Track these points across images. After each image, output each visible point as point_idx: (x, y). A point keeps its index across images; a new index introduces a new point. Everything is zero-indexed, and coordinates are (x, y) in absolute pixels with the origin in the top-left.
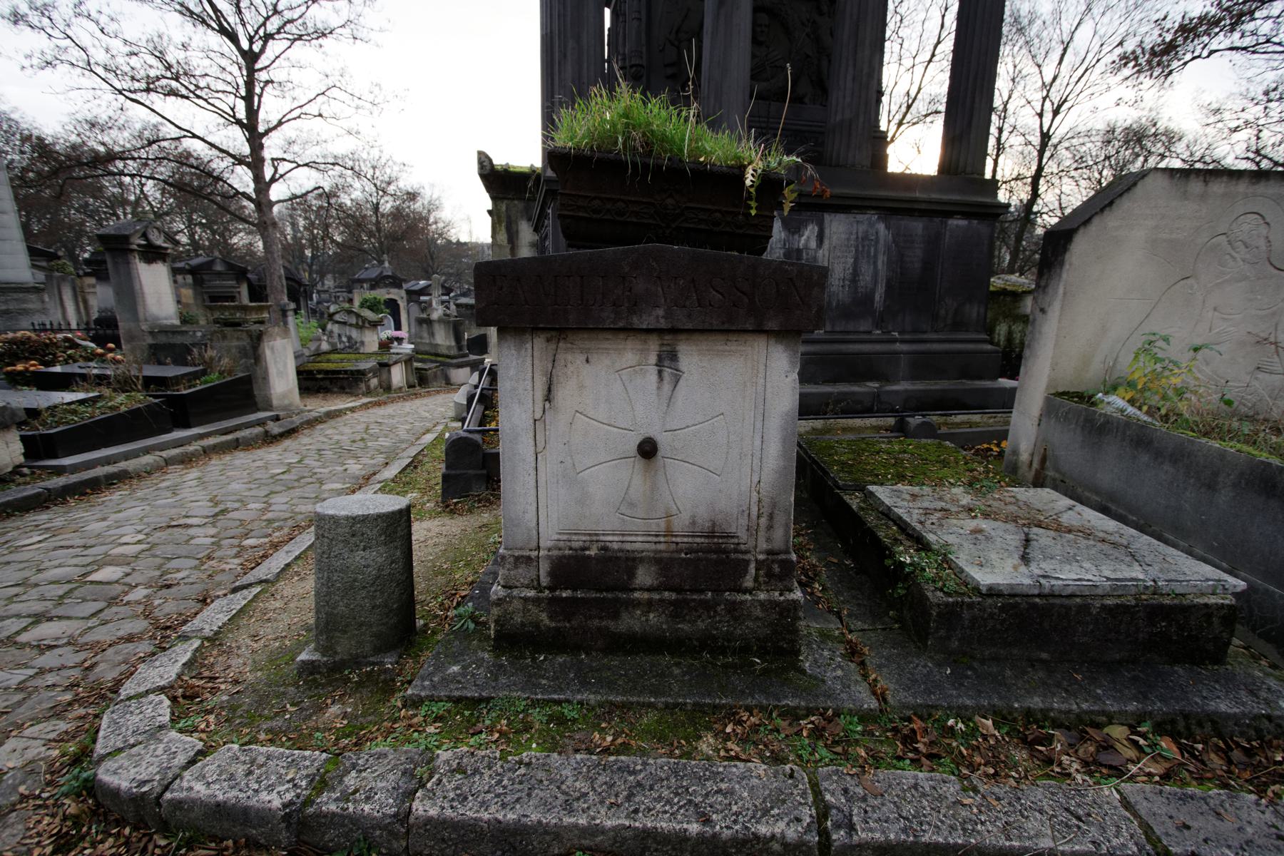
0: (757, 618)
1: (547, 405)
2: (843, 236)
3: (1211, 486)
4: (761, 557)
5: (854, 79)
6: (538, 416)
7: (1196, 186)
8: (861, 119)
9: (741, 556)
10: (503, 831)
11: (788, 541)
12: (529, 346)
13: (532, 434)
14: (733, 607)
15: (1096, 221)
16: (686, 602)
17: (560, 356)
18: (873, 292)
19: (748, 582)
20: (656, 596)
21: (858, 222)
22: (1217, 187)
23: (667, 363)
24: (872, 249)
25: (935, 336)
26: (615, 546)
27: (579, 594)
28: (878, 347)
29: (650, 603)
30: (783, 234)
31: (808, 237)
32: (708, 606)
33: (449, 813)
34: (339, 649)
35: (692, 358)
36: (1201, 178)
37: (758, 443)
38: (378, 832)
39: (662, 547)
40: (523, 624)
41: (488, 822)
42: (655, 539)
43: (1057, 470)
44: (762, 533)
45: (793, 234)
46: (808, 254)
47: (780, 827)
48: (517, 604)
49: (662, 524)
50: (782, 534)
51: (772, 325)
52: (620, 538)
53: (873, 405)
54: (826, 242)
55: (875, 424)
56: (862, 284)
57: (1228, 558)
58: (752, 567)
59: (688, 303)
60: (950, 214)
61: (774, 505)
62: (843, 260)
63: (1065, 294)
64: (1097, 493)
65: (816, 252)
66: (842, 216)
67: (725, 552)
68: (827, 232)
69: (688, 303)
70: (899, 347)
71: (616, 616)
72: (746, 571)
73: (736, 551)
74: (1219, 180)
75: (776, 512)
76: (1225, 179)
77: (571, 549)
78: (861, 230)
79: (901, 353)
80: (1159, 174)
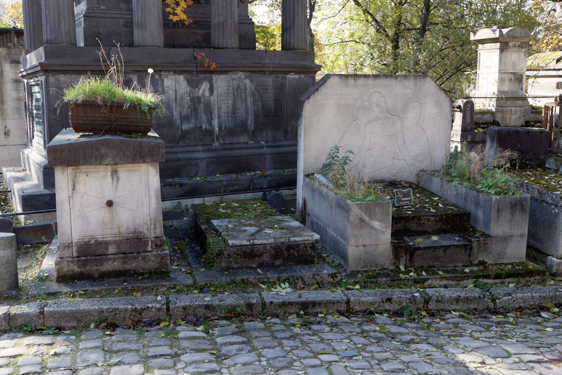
0: (153, 261)
1: (73, 191)
2: (225, 88)
4: (153, 239)
6: (70, 195)
7: (351, 81)
8: (229, 21)
9: (146, 239)
10: (73, 313)
11: (162, 233)
12: (66, 172)
13: (68, 202)
17: (78, 175)
18: (246, 119)
19: (149, 249)
20: (117, 256)
21: (233, 79)
22: (360, 81)
23: (114, 175)
24: (243, 94)
25: (286, 143)
27: (88, 258)
28: (252, 151)
30: (188, 89)
31: (204, 90)
33: (56, 309)
35: (124, 171)
36: (353, 78)
38: (34, 318)
39: (117, 238)
40: (68, 271)
42: (115, 236)
45: (195, 88)
46: (204, 99)
50: (159, 231)
52: (102, 236)
53: (250, 186)
54: (215, 92)
55: (252, 197)
56: (239, 115)
58: (150, 242)
59: (120, 156)
60: (288, 73)
61: (155, 220)
62: (226, 102)
63: (304, 129)
65: (209, 98)
66: (223, 76)
67: (141, 239)
68: (215, 86)
69: (120, 156)
70: (265, 150)
71: (102, 264)
72: (148, 245)
73: (144, 238)
74: (360, 79)
75: (156, 223)
76: (363, 78)
77: (84, 242)
78: (235, 84)
79: (266, 154)
80: (335, 77)
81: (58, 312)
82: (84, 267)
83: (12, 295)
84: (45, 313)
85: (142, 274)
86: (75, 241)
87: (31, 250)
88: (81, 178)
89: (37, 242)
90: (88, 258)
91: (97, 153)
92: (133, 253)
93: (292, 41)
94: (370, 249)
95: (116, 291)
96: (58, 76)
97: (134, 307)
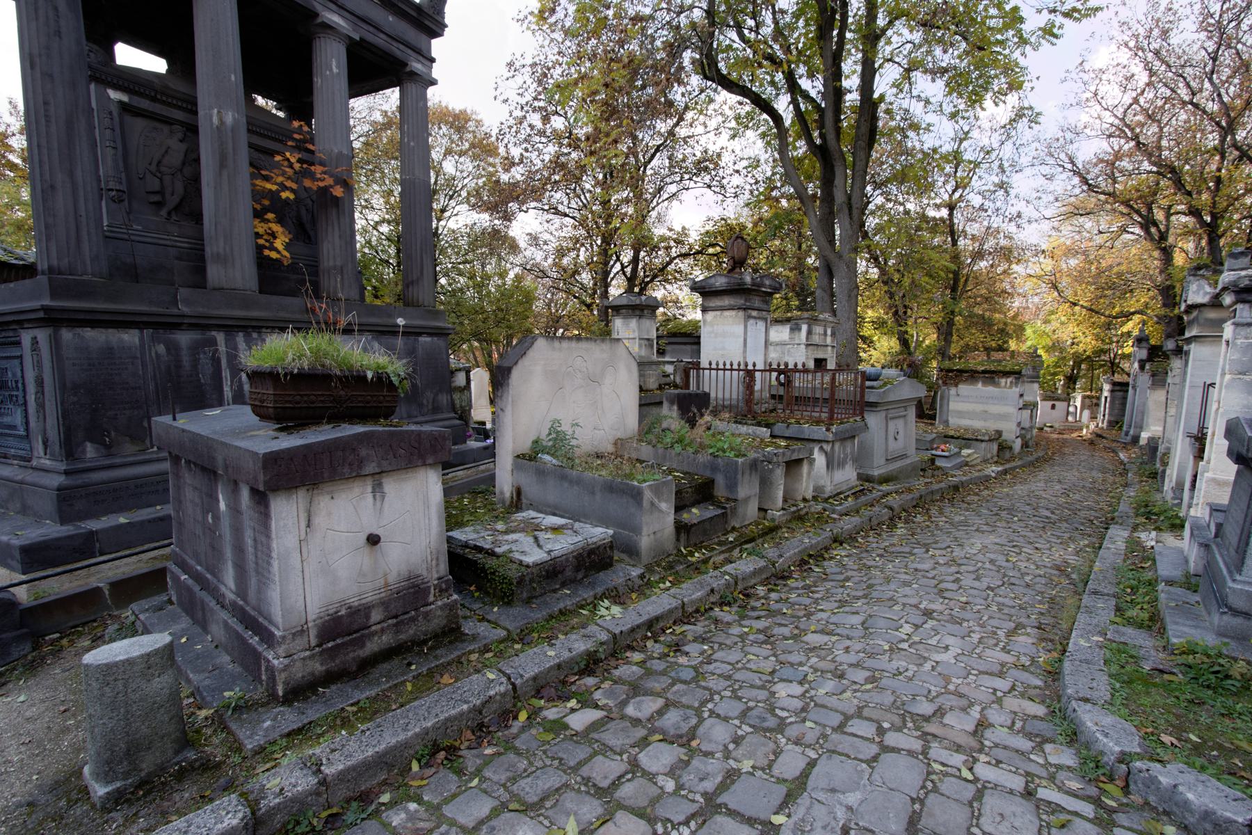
3: (593, 493)
4: (436, 582)
5: (340, 237)
14: (427, 614)
15: (520, 362)
16: (402, 621)
19: (431, 599)
26: (356, 604)
27: (339, 641)
29: (383, 630)
32: (413, 619)
33: (349, 763)
34: (144, 766)
35: (391, 486)
37: (427, 521)
39: (383, 595)
40: (303, 677)
41: (372, 756)
43: (527, 499)
44: (434, 570)
47: (497, 689)
48: (298, 664)
49: (382, 582)
51: (430, 461)
57: (603, 521)
60: (420, 334)
61: (438, 552)
64: (549, 507)
67: (418, 586)
71: (363, 646)
73: (423, 583)
81: (353, 768)
82: (332, 659)
83: (191, 764)
84: (329, 779)
85: (425, 642)
86: (311, 617)
87: (65, 642)
88: (322, 504)
89: (71, 624)
90: (339, 641)
91: (352, 457)
92: (408, 613)
93: (415, 295)
94: (659, 535)
95: (409, 687)
96: (79, 330)
97: (471, 705)
